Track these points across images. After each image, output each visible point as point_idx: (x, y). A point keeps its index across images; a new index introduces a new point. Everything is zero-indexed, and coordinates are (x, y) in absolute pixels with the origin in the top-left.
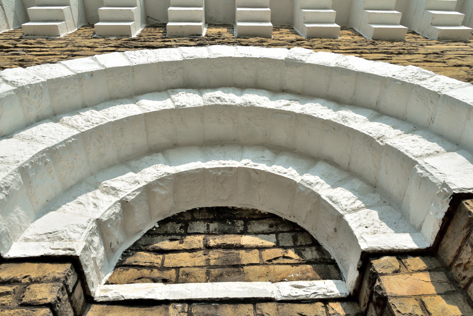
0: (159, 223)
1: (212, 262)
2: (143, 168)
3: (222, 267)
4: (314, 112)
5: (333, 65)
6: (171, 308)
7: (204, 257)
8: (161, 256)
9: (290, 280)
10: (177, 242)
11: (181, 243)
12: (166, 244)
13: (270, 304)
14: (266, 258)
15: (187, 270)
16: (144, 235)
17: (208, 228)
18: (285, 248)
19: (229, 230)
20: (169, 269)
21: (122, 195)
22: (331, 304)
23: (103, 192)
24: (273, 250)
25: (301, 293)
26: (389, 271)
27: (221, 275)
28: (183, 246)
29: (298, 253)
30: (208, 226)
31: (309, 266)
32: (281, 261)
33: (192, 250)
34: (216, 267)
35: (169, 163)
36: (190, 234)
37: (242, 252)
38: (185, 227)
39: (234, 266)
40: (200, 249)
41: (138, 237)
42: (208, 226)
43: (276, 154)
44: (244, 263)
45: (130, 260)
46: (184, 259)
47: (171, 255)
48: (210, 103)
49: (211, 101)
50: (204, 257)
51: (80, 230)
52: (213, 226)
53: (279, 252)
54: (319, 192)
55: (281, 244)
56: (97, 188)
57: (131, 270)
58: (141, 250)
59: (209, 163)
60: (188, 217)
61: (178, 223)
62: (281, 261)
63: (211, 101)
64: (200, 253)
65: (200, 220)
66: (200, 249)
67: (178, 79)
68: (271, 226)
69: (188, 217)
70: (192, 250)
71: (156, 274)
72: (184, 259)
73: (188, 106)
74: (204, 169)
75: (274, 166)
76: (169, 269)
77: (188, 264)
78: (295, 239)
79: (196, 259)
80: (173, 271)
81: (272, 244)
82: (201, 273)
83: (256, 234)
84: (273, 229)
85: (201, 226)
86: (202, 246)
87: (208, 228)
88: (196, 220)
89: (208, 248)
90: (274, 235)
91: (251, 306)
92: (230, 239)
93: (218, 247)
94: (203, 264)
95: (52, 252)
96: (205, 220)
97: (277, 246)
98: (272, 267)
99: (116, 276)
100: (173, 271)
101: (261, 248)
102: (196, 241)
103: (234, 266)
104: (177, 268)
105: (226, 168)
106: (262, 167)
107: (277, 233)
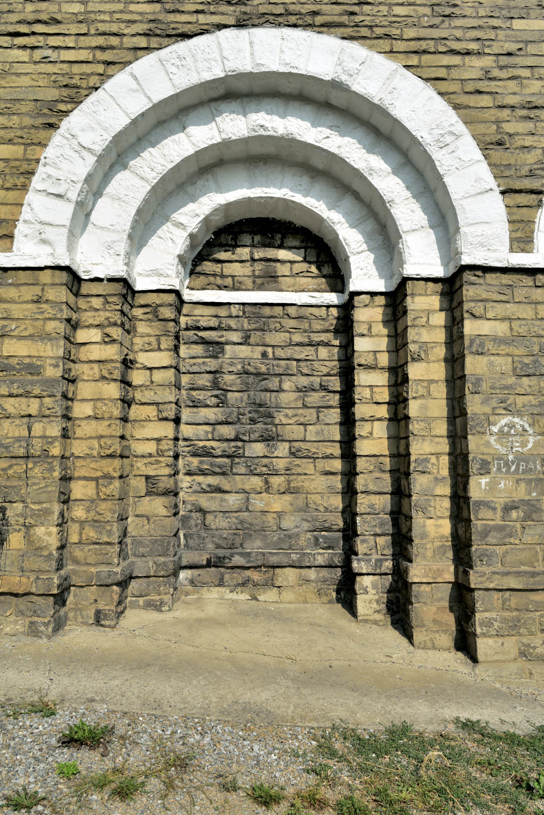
0: (214, 233)
1: (257, 273)
2: (199, 197)
3: (264, 277)
4: (348, 156)
5: (376, 101)
6: (232, 307)
7: (251, 268)
8: (219, 265)
9: (309, 291)
10: (230, 253)
11: (233, 254)
12: (223, 255)
13: (293, 307)
14: (295, 272)
15: (240, 279)
16: (204, 246)
17: (253, 241)
18: (310, 263)
19: (270, 243)
20: (227, 277)
21: (189, 230)
22: (331, 309)
23: (174, 225)
24: (300, 264)
25: (313, 301)
26: (361, 305)
27: (263, 284)
28: (234, 257)
29: (318, 268)
30: (253, 238)
31: (324, 280)
32: (305, 274)
33: (242, 262)
34: (259, 277)
35: (220, 190)
36: (239, 246)
37: (278, 265)
38: (235, 239)
39: (272, 277)
40: (247, 261)
41: (200, 248)
42: (253, 238)
43: (312, 178)
44: (279, 274)
45: (198, 269)
46: (236, 269)
47: (227, 264)
48: (254, 134)
49: (255, 131)
50: (251, 268)
51: (171, 267)
52: (257, 238)
53: (305, 266)
54: (338, 232)
55: (308, 259)
56: (167, 221)
57: (202, 278)
58: (205, 260)
59: (254, 190)
60: (237, 229)
61: (229, 235)
62: (305, 274)
63: (255, 131)
64: (248, 264)
65: (246, 232)
66: (247, 261)
67: (221, 91)
68: (302, 242)
69: (237, 229)
70: (242, 262)
71: (219, 281)
72: (236, 269)
73: (234, 138)
74: (250, 198)
75: (308, 198)
76: (227, 277)
77: (240, 274)
78: (318, 256)
79: (245, 269)
80: (230, 278)
81: (301, 259)
82: (249, 282)
83: (290, 248)
84: (303, 245)
85: (246, 239)
86: (249, 258)
87: (253, 241)
88: (243, 232)
89: (253, 260)
90: (303, 250)
91: (281, 308)
92: (271, 253)
93: (261, 260)
94: (250, 274)
95: (163, 287)
96: (250, 233)
97: (305, 260)
98: (298, 279)
99: (192, 283)
100: (230, 278)
101: (292, 262)
102: (244, 252)
103: (272, 277)
104: (233, 277)
105: (268, 197)
106: (299, 198)
107: (306, 248)
